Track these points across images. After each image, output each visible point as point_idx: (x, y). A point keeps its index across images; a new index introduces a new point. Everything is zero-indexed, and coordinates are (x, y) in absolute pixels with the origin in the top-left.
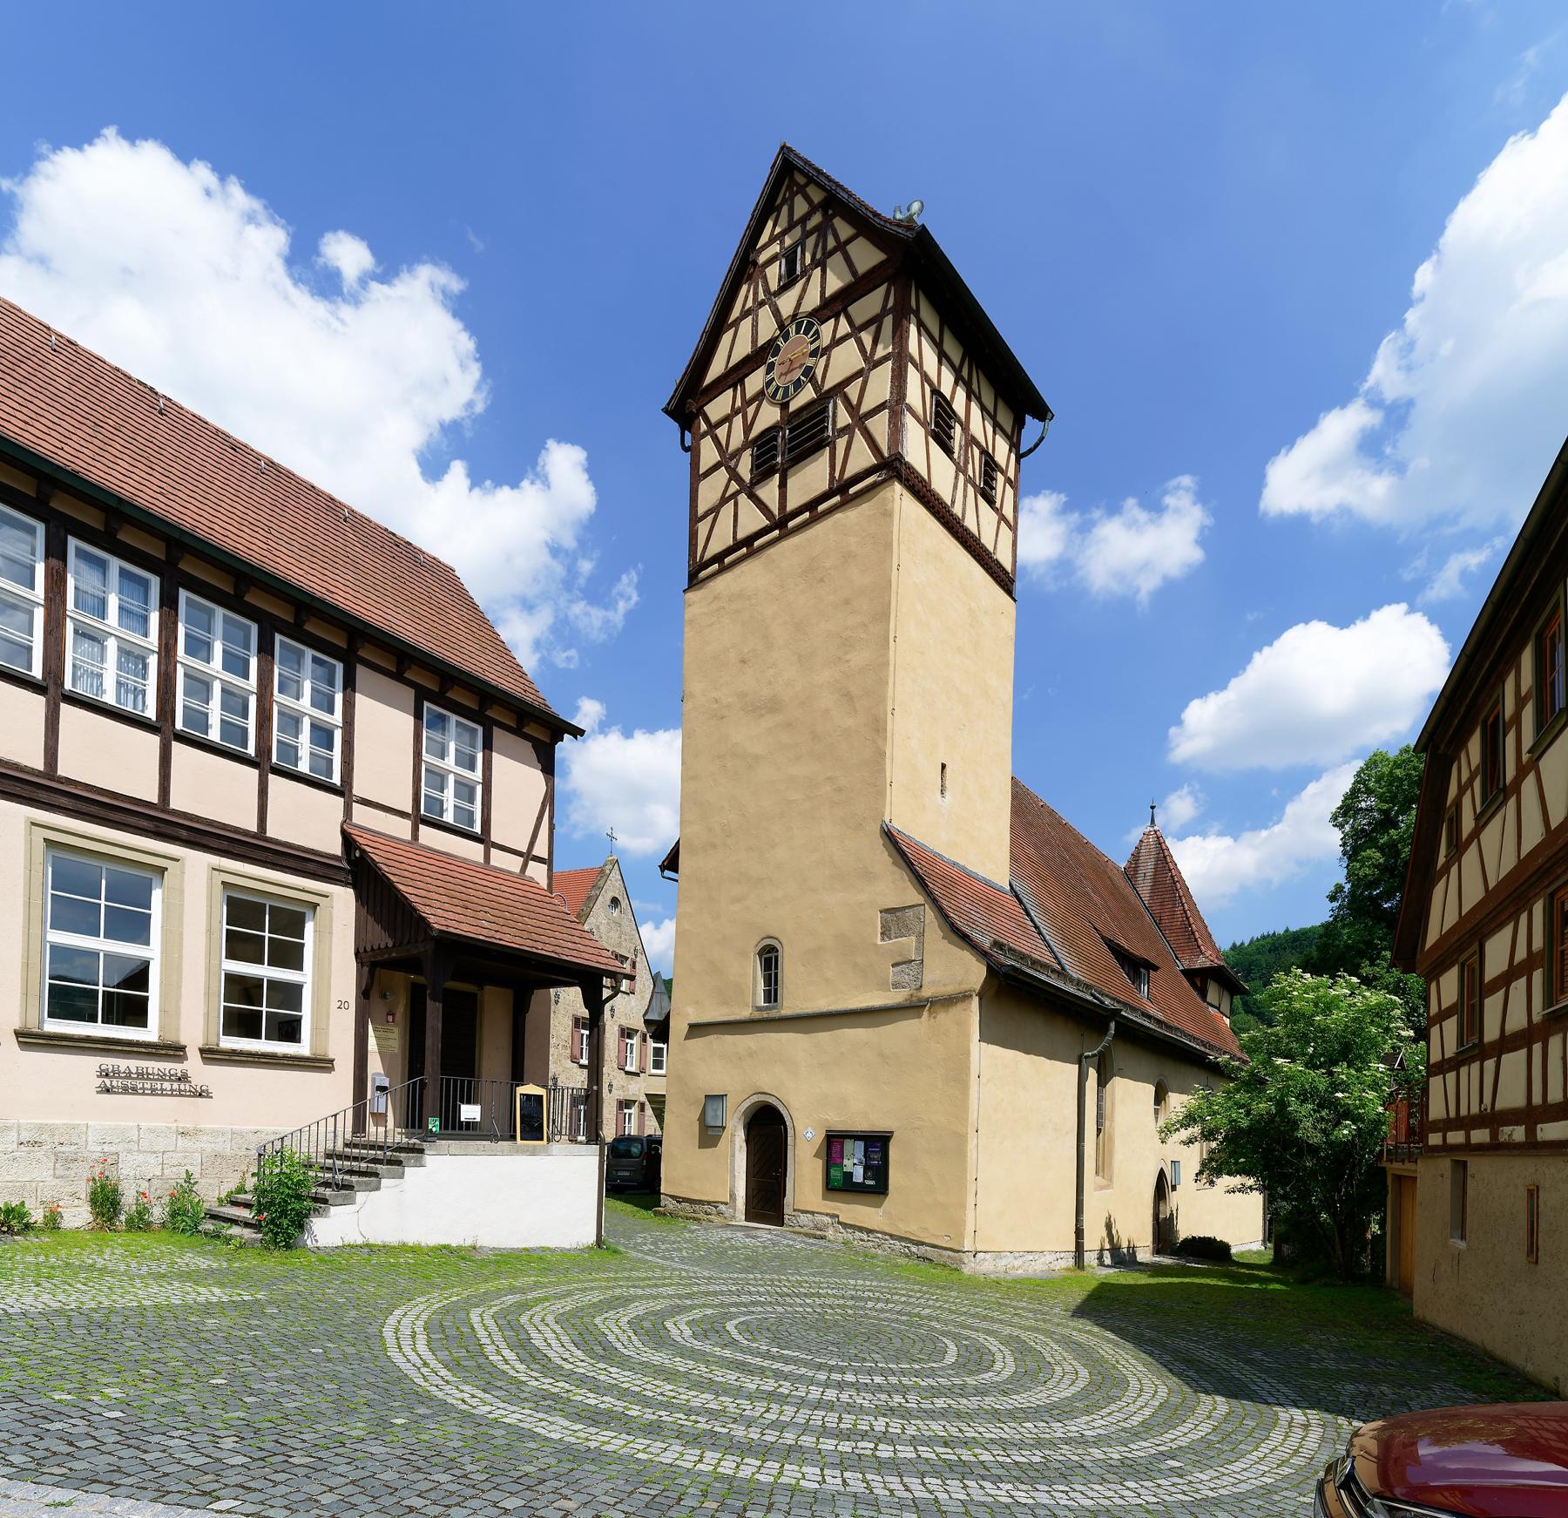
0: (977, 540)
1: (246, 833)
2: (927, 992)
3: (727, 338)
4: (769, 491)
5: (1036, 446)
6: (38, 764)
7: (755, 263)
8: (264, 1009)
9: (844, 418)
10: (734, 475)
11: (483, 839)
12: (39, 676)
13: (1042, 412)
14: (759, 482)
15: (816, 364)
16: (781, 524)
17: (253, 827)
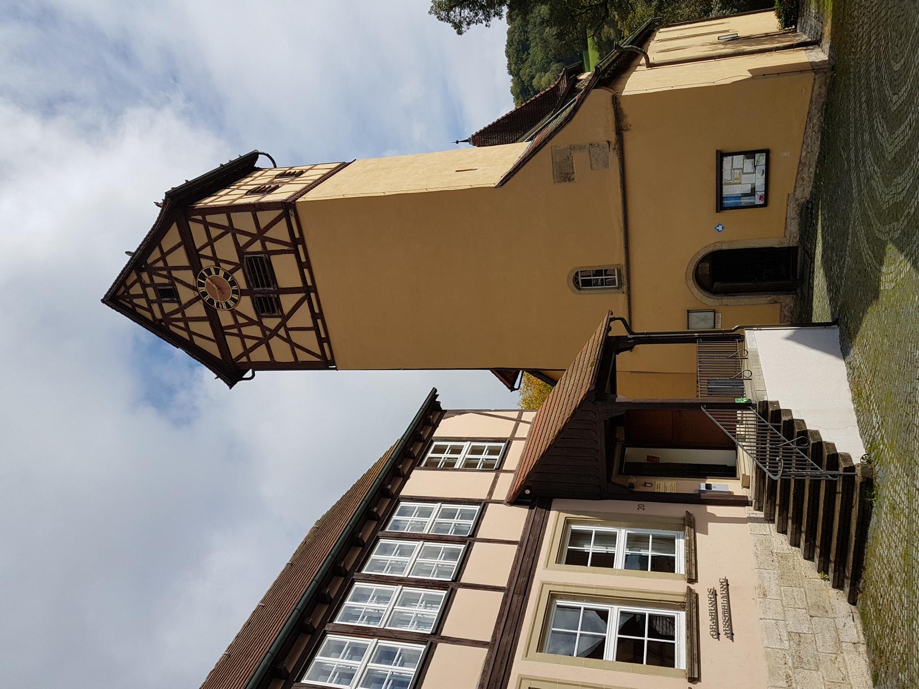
0: (325, 175)
1: (519, 551)
2: (613, 137)
3: (198, 341)
4: (287, 302)
5: (271, 158)
6: (485, 651)
10: (274, 333)
11: (484, 505)
12: (425, 646)
13: (254, 156)
15: (223, 269)
16: (308, 290)
17: (515, 547)
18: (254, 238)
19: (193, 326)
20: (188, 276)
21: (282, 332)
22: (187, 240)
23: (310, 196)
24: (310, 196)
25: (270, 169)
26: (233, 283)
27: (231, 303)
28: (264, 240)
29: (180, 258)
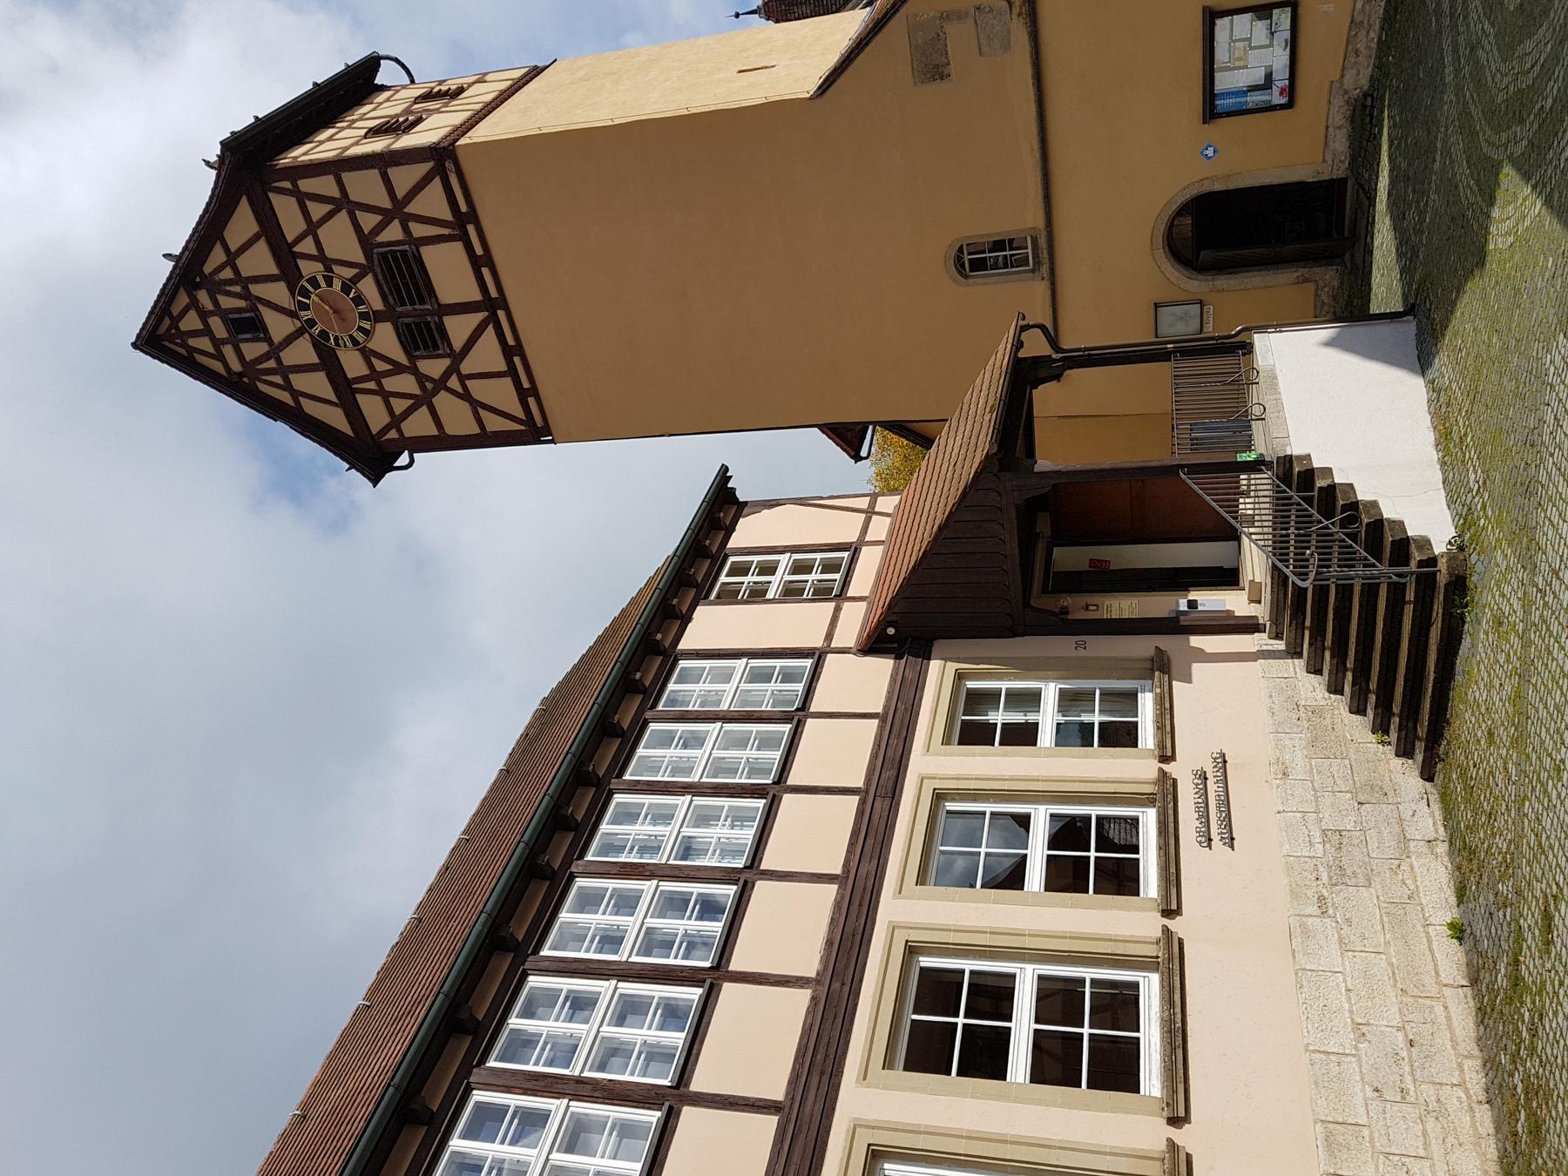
0: (503, 92)
4: (458, 328)
7: (240, 375)
8: (1086, 1031)
9: (394, 232)
14: (450, 345)
15: (340, 277)
16: (493, 306)
18: (387, 216)
19: (300, 382)
20: (278, 292)
21: (454, 383)
22: (269, 227)
23: (483, 133)
24: (483, 133)
25: (404, 87)
26: (359, 300)
27: (360, 337)
28: (405, 220)
29: (260, 260)
